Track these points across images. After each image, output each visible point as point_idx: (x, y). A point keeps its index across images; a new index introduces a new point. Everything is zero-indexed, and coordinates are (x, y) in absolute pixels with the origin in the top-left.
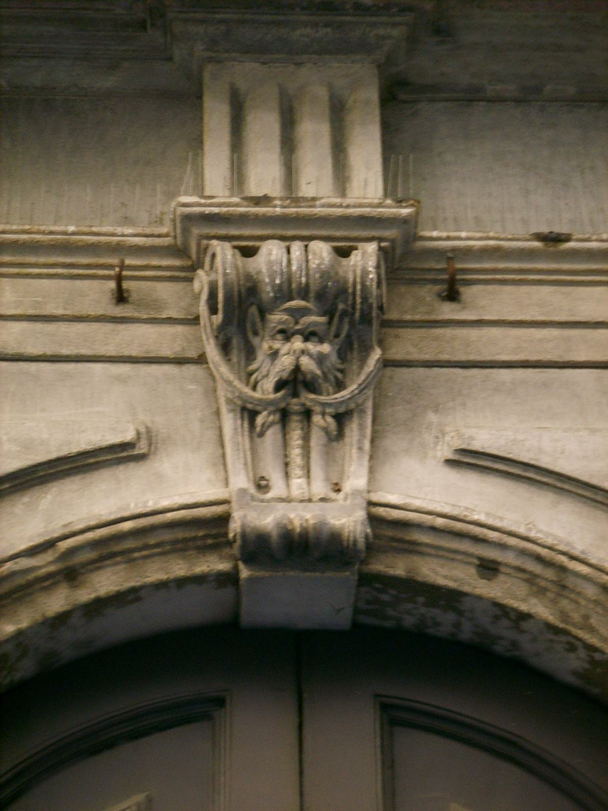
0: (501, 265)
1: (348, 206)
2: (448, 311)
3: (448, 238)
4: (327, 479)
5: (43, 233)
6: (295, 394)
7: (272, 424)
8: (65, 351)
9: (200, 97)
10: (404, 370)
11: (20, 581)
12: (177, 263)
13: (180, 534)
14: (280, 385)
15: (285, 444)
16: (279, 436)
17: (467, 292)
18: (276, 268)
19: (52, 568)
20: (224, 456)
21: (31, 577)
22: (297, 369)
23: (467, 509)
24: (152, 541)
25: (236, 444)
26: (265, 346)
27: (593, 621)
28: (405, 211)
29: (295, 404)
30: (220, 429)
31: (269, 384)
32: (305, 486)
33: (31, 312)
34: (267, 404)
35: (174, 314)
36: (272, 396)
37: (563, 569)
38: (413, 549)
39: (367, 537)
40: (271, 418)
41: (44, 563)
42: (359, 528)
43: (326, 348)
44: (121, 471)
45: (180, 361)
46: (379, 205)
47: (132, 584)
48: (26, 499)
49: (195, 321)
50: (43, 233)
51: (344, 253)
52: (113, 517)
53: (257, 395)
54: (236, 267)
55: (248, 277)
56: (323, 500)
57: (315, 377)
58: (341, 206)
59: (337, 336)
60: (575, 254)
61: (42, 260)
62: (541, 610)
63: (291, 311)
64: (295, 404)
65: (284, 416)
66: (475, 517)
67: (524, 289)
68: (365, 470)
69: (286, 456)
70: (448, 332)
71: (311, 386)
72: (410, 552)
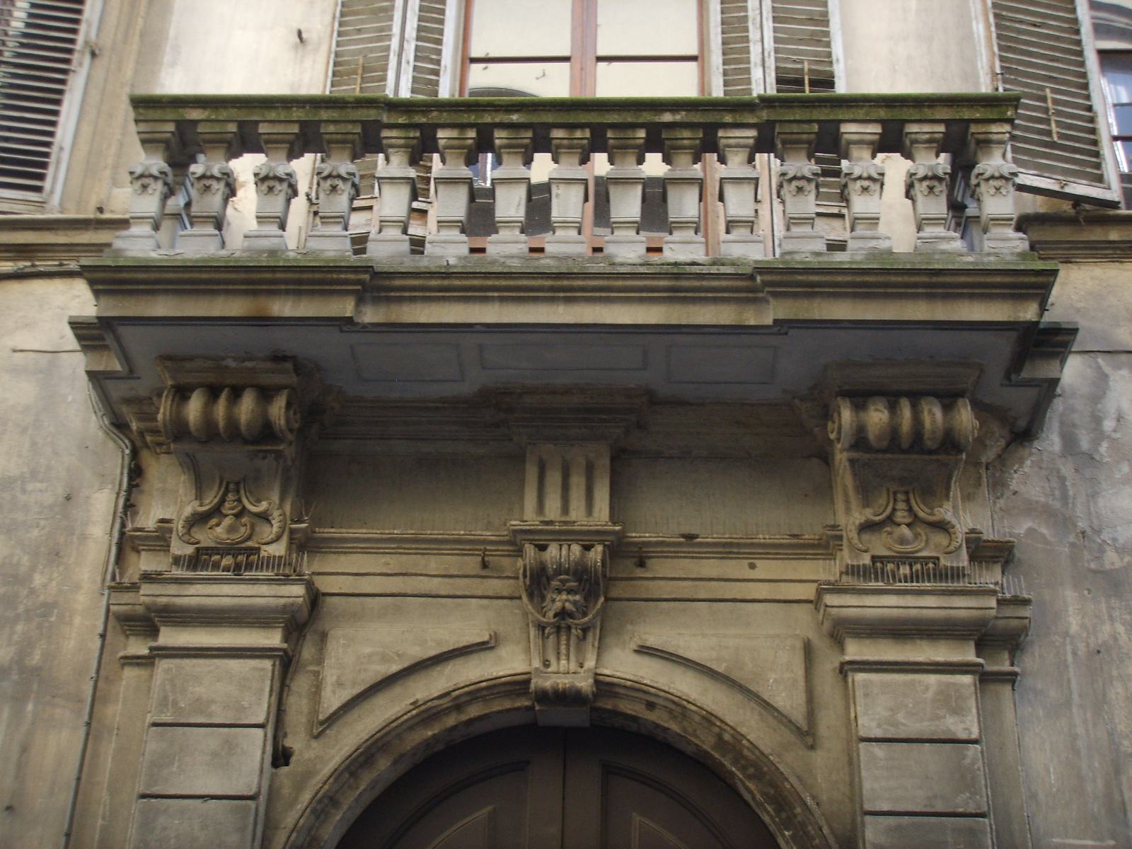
0: (666, 549)
1: (590, 526)
2: (639, 572)
3: (640, 537)
4: (577, 661)
5: (449, 535)
6: (564, 619)
7: (553, 633)
8: (459, 593)
9: (525, 461)
10: (619, 602)
11: (434, 711)
12: (511, 548)
13: (508, 688)
14: (555, 616)
15: (558, 643)
16: (556, 640)
17: (649, 562)
18: (554, 560)
19: (449, 705)
20: (530, 647)
21: (439, 709)
22: (564, 608)
23: (641, 677)
24: (495, 691)
25: (535, 643)
26: (549, 596)
27: (698, 733)
28: (617, 528)
29: (563, 624)
30: (529, 633)
31: (551, 614)
32: (566, 665)
33: (443, 573)
34: (549, 624)
35: (509, 575)
36: (552, 620)
37: (685, 708)
38: (616, 696)
39: (593, 692)
40: (552, 630)
41: (445, 702)
42: (589, 689)
43: (577, 597)
44: (483, 655)
45: (511, 598)
46: (606, 525)
47: (486, 712)
48: (439, 669)
49: (517, 578)
50: (449, 535)
51: (587, 548)
52: (476, 681)
53: (545, 620)
54: (535, 559)
55: (542, 563)
56: (574, 673)
57: (572, 612)
58: (586, 526)
59: (583, 590)
60: (701, 544)
61: (448, 547)
62: (674, 727)
63: (561, 581)
64: (563, 624)
65: (558, 629)
66: (645, 682)
67: (676, 560)
68: (595, 657)
69: (559, 649)
70: (639, 583)
71: (571, 615)
72: (615, 697)
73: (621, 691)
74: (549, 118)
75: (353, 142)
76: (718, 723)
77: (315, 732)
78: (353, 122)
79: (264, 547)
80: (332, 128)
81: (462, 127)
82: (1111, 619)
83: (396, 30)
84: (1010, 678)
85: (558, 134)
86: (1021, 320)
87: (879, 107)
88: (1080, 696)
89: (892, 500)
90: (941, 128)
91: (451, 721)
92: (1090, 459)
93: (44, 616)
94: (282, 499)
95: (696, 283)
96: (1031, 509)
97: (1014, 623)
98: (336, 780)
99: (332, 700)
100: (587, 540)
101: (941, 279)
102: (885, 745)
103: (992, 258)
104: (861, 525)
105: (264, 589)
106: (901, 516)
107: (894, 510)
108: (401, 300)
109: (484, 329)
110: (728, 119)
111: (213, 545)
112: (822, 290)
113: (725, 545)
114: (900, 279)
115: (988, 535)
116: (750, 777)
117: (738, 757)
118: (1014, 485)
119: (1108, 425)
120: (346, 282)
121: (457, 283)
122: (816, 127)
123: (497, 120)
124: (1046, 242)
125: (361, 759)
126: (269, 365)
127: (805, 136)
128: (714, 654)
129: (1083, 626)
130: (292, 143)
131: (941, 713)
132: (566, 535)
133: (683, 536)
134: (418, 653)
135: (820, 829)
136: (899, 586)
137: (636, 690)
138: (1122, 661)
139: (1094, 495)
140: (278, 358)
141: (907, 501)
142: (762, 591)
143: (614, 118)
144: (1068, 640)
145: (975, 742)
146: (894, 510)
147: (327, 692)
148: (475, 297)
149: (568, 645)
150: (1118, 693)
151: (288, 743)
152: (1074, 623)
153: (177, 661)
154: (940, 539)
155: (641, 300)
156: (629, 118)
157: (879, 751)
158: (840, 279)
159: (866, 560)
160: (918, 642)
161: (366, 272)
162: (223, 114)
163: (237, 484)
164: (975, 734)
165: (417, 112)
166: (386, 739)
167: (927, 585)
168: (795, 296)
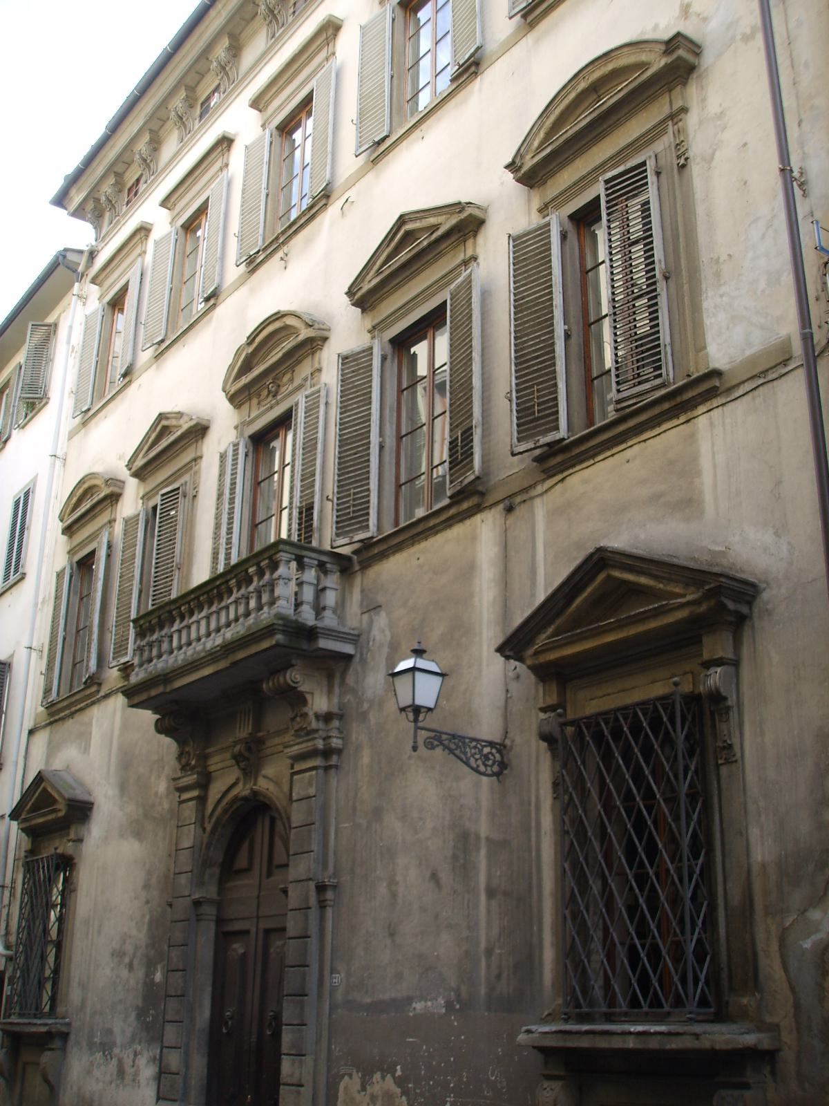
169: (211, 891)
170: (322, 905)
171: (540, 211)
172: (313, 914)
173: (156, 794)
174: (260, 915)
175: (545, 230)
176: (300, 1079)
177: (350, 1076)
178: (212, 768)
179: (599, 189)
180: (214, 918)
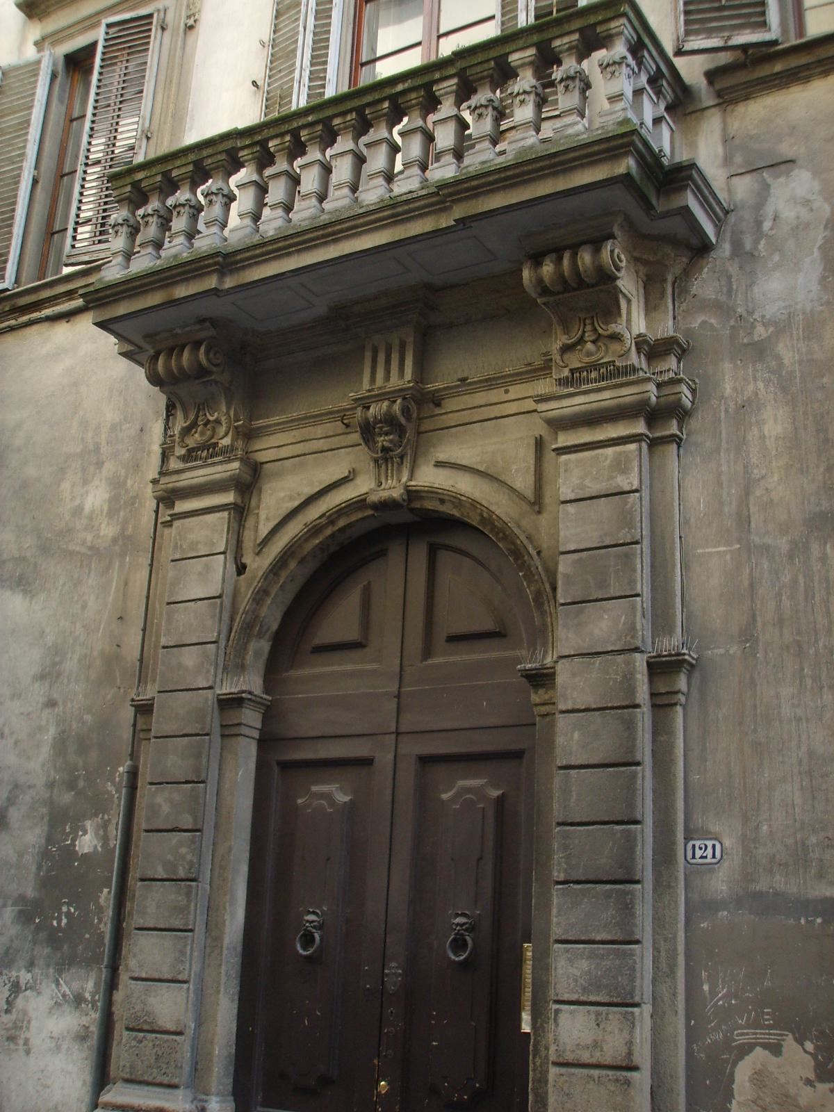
2: (438, 411)
37: (459, 499)
38: (422, 498)
41: (323, 520)
43: (391, 437)
44: (347, 485)
54: (361, 417)
63: (379, 428)
65: (386, 460)
67: (460, 397)
73: (423, 494)
74: (329, 112)
75: (223, 166)
76: (478, 506)
77: (257, 551)
78: (220, 153)
79: (220, 441)
80: (210, 161)
81: (282, 135)
82: (755, 379)
83: (298, 64)
84: (676, 440)
85: (337, 121)
86: (616, 175)
87: (532, 34)
88: (727, 442)
89: (582, 325)
90: (576, 36)
91: (328, 532)
92: (752, 256)
93: (133, 504)
94: (228, 409)
95: (406, 208)
96: (704, 306)
97: (672, 398)
98: (265, 580)
99: (264, 530)
100: (391, 396)
101: (557, 160)
102: (574, 504)
103: (600, 132)
104: (561, 348)
105: (219, 468)
106: (589, 336)
107: (584, 332)
108: (244, 268)
109: (291, 274)
110: (437, 76)
111: (195, 445)
112: (482, 190)
113: (486, 380)
114: (530, 168)
115: (652, 337)
116: (500, 540)
117: (493, 527)
118: (694, 290)
119: (767, 225)
120: (209, 266)
121: (270, 248)
122: (492, 63)
123: (300, 124)
124: (727, 88)
125: (279, 565)
126: (198, 327)
127: (486, 73)
128: (479, 459)
129: (735, 389)
130: (191, 178)
131: (614, 474)
132: (380, 397)
133: (459, 380)
134: (309, 490)
135: (537, 568)
136: (584, 387)
137: (432, 493)
138: (759, 410)
139: (750, 285)
140: (201, 321)
141: (593, 324)
142: (513, 408)
143: (368, 99)
144: (723, 401)
145: (636, 491)
146: (584, 332)
147: (261, 526)
148: (282, 254)
149: (392, 470)
150: (754, 436)
151: (244, 560)
152: (728, 388)
153: (182, 521)
154: (615, 347)
155: (377, 229)
156: (376, 96)
157: (571, 508)
158: (491, 179)
159: (566, 373)
160: (605, 425)
161: (218, 256)
162: (154, 171)
163: (204, 404)
164: (635, 485)
165: (255, 133)
166: (293, 549)
167: (603, 384)
168: (466, 198)
169: (252, 682)
170: (662, 704)
171: (36, 44)
172: (644, 717)
173: (78, 511)
174: (402, 729)
175: (39, 62)
176: (630, 1054)
177: (776, 1049)
178: (262, 457)
179: (99, 34)
180: (256, 734)
